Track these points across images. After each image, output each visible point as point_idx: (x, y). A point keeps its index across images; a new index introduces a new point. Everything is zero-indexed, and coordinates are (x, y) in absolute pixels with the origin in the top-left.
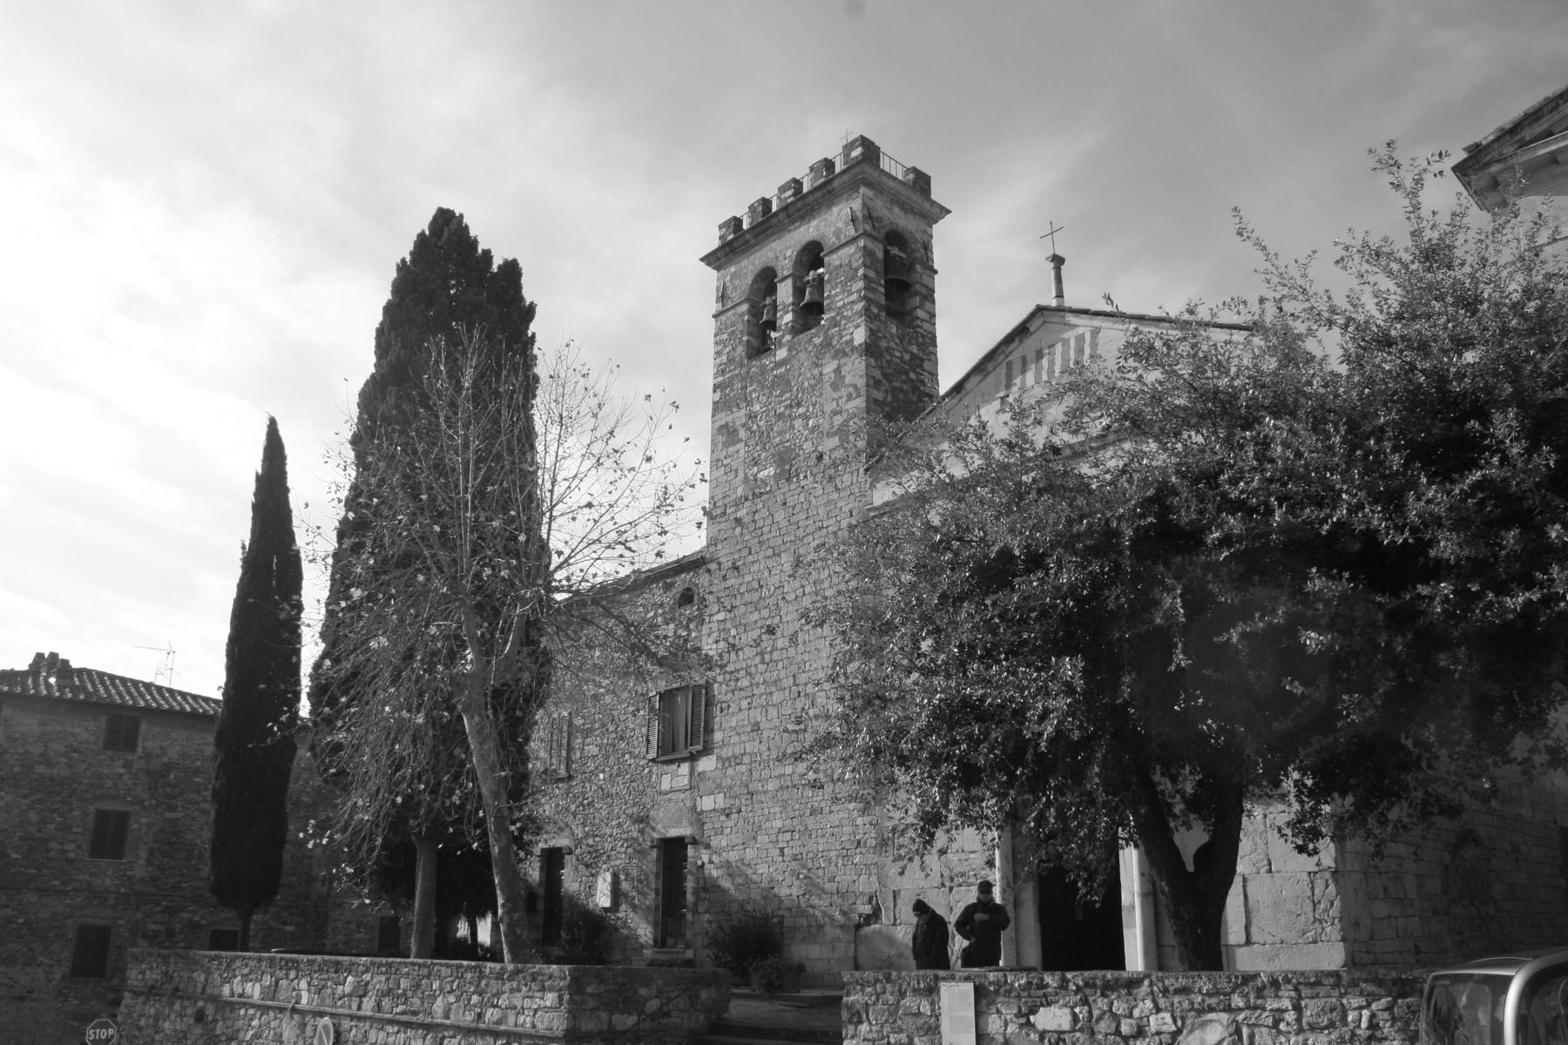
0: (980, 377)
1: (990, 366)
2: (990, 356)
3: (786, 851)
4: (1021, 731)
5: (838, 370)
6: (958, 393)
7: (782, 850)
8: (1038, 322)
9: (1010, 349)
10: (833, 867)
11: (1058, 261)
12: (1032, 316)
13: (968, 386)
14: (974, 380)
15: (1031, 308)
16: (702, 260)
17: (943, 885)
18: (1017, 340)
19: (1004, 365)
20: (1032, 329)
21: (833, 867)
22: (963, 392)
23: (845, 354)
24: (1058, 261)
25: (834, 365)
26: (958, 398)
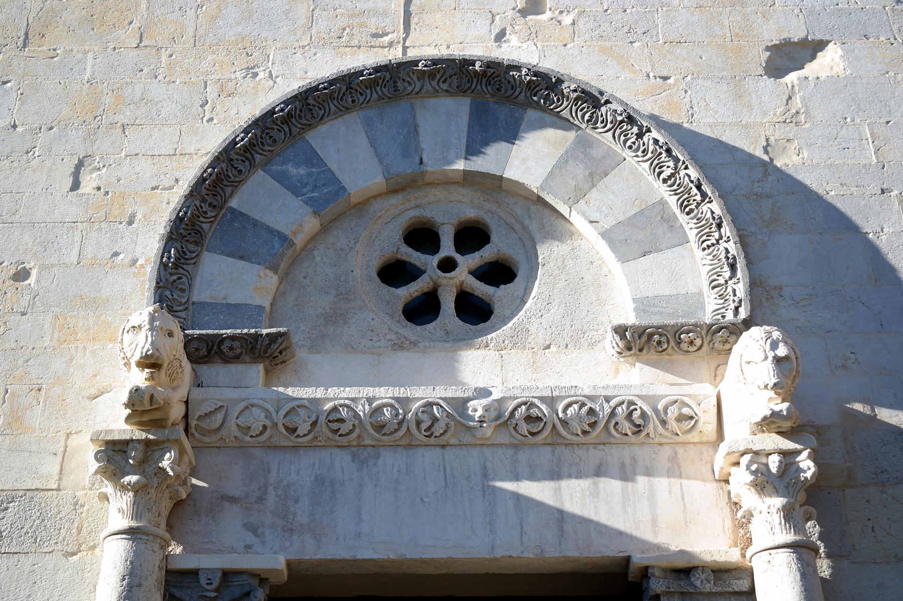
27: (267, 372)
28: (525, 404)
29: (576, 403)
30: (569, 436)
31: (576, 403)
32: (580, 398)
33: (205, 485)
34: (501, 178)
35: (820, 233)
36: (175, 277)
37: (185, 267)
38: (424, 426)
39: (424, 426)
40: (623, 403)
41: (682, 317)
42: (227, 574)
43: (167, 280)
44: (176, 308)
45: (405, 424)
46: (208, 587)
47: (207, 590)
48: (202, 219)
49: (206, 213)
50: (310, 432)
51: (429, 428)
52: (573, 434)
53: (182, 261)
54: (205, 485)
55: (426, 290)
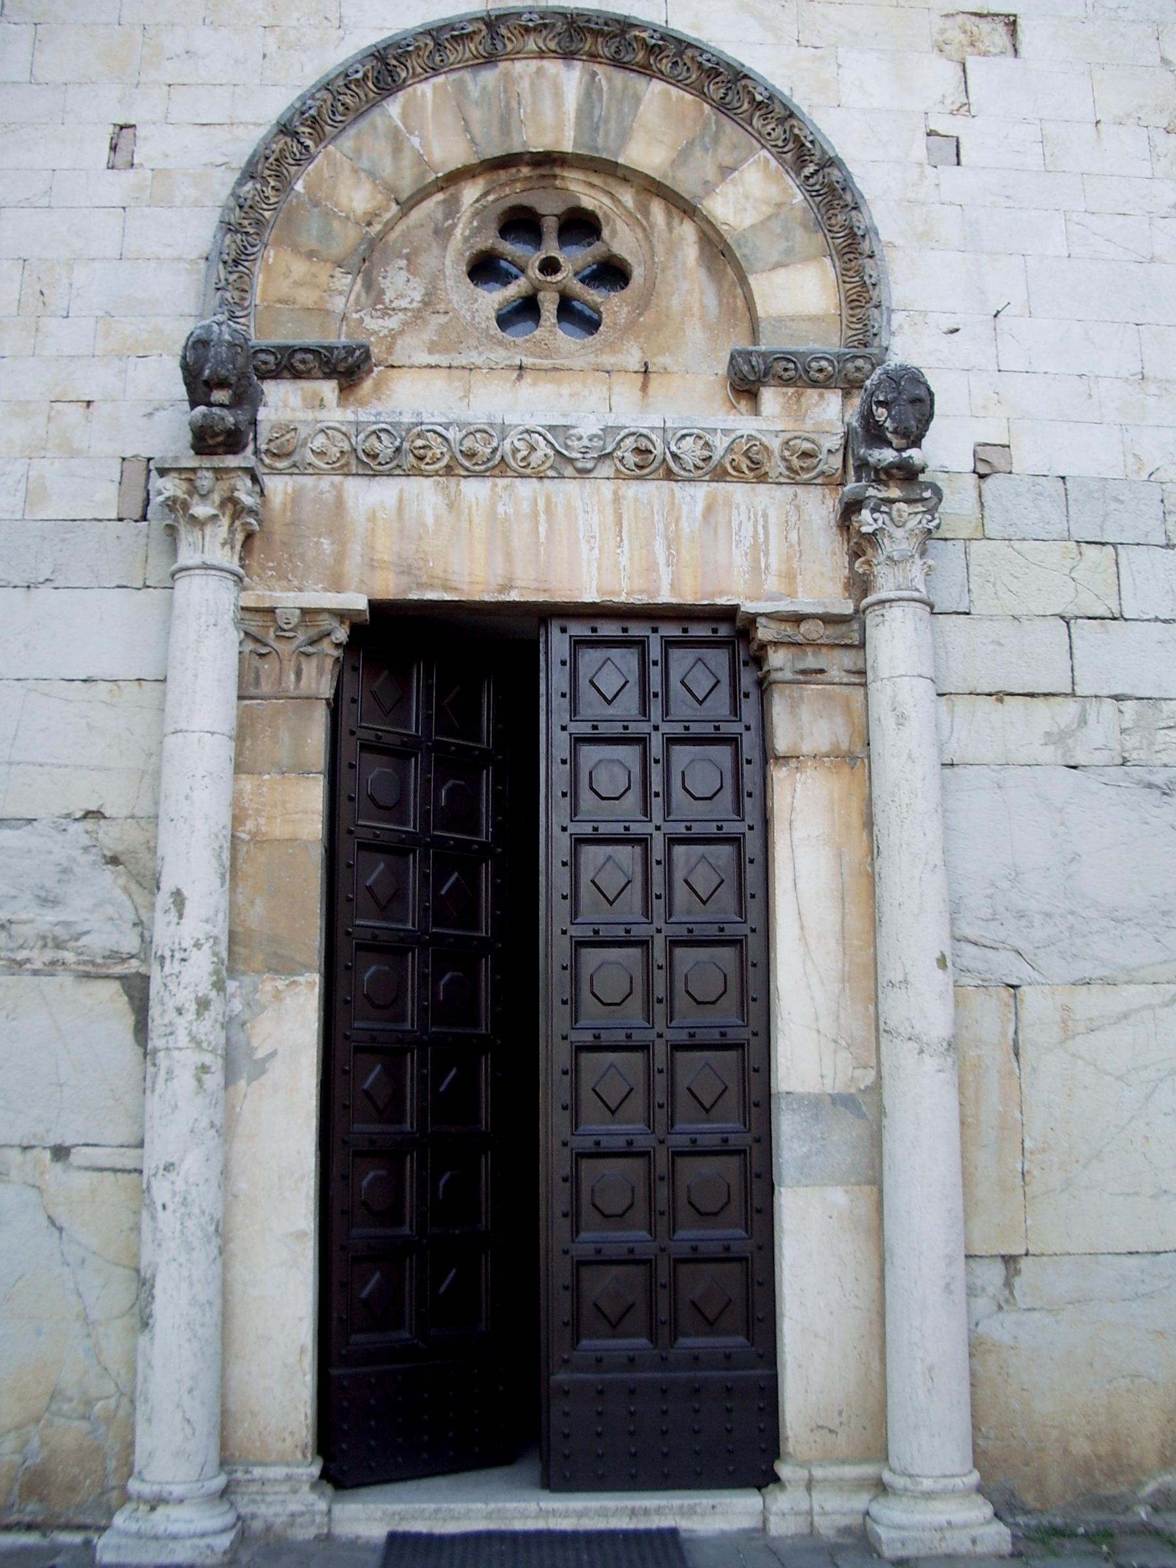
27: (341, 390)
28: (633, 434)
29: (690, 435)
30: (682, 473)
31: (690, 435)
32: (695, 431)
33: (454, 1271)
34: (616, 163)
35: (697, 1453)
36: (235, 276)
37: (246, 264)
38: (520, 456)
39: (520, 456)
40: (742, 437)
41: (814, 341)
42: (305, 612)
43: (226, 280)
44: (238, 314)
45: (499, 454)
46: (286, 627)
47: (285, 630)
48: (265, 206)
49: (267, 198)
50: (392, 460)
51: (524, 459)
52: (684, 469)
53: (243, 257)
54: (454, 1271)
55: (524, 294)
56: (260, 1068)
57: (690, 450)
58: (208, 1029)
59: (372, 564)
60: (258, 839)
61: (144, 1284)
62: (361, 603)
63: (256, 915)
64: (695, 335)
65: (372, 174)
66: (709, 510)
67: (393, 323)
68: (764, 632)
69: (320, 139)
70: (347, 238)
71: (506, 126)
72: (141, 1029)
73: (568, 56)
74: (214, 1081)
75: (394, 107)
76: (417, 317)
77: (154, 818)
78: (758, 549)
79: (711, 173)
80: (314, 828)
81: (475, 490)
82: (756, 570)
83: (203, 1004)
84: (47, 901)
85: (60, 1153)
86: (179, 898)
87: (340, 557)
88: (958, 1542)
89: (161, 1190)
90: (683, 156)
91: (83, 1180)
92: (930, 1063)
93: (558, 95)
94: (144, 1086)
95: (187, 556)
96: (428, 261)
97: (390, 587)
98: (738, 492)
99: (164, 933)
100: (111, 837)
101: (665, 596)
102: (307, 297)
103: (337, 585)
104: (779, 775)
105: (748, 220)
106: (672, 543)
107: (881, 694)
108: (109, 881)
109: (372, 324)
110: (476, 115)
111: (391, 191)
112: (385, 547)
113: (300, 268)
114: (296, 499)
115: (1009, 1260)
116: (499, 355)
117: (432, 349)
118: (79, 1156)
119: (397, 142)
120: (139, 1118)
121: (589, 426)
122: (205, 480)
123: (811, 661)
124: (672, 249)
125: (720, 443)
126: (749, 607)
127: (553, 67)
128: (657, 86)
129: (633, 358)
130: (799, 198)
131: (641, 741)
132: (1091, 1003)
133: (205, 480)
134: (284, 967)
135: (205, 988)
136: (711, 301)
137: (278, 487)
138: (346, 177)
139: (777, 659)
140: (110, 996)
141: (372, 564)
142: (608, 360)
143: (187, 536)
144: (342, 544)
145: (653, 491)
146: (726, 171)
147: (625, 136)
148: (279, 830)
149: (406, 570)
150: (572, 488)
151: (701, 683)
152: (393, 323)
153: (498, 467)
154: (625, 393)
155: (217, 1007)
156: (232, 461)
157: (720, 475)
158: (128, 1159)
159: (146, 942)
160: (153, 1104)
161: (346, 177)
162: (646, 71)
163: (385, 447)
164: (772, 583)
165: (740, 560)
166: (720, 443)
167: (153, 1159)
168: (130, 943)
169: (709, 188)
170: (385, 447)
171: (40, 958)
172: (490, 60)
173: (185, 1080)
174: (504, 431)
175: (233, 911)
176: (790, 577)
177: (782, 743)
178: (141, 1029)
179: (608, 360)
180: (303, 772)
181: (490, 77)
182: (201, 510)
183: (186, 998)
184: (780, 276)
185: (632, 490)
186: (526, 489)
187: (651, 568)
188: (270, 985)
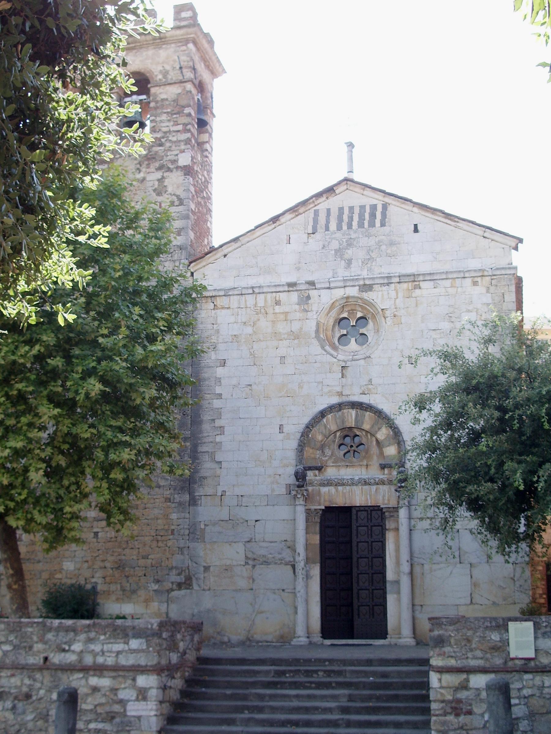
0: (293, 215)
1: (301, 210)
2: (304, 203)
3: (100, 535)
4: (39, 148)
5: (161, 180)
6: (274, 223)
7: (96, 534)
8: (342, 188)
9: (318, 201)
10: (147, 548)
11: (351, 145)
12: (339, 183)
13: (283, 219)
14: (288, 216)
15: (342, 178)
16: (346, 143)
17: (247, 563)
18: (325, 195)
19: (312, 211)
20: (337, 192)
21: (147, 548)
22: (278, 223)
23: (169, 170)
24: (351, 145)
25: (159, 175)
26: (273, 226)
56: (312, 577)
57: (372, 481)
58: (304, 572)
59: (325, 501)
60: (310, 544)
61: (296, 608)
62: (323, 508)
63: (310, 555)
64: (375, 458)
65: (322, 433)
66: (376, 490)
67: (327, 458)
68: (384, 510)
69: (313, 427)
70: (318, 445)
71: (343, 422)
72: (294, 572)
73: (353, 408)
74: (305, 580)
75: (325, 420)
76: (330, 457)
77: (295, 541)
78: (384, 496)
79: (377, 429)
80: (318, 542)
81: (340, 488)
82: (383, 499)
83: (303, 569)
84: (280, 553)
85: (283, 590)
86: (299, 554)
87: (320, 500)
88: (408, 644)
89: (298, 595)
90: (372, 426)
91: (286, 594)
92: (405, 576)
93: (351, 416)
94: (295, 580)
95: (297, 503)
96: (332, 447)
97: (328, 504)
98: (381, 487)
99: (297, 559)
100: (288, 544)
101: (369, 505)
102: (313, 456)
103: (320, 505)
104: (387, 532)
105: (383, 438)
106: (370, 496)
107: (400, 521)
108: (288, 551)
109: (323, 459)
110: (338, 421)
111: (325, 436)
112: (327, 498)
113: (311, 451)
114: (313, 490)
115: (421, 606)
116: (343, 463)
117: (333, 463)
118: (286, 591)
119: (325, 427)
120: (295, 585)
121: (357, 478)
122: (299, 491)
123: (392, 514)
124: (372, 442)
125: (377, 480)
126: (382, 506)
127: (350, 410)
128: (368, 413)
129: (365, 463)
130: (392, 433)
131: (367, 526)
132: (435, 567)
133: (299, 491)
134: (314, 563)
135: (303, 566)
136: (378, 452)
137: (310, 489)
138: (318, 434)
139: (386, 514)
140: (289, 568)
141: (325, 501)
142: (361, 463)
143: (297, 500)
144: (320, 498)
145: (366, 487)
146: (379, 429)
147: (363, 423)
148: (313, 542)
149: (330, 501)
150: (355, 487)
151: (377, 516)
152: (327, 458)
153: (343, 485)
154: (364, 470)
155: (305, 569)
156: (303, 489)
157: (378, 484)
158: (293, 591)
159: (294, 559)
160: (297, 583)
161: (318, 434)
162: (366, 410)
163: (326, 482)
164: (386, 502)
165: (381, 498)
166: (377, 480)
167: (297, 590)
168: (292, 559)
169: (376, 432)
170: (326, 482)
171: (279, 562)
172: (340, 410)
173: (301, 579)
174: (344, 479)
175: (307, 555)
176: (389, 500)
177: (387, 527)
178: (294, 572)
179: (361, 463)
180: (316, 533)
181: (340, 413)
182: (299, 496)
183: (300, 568)
184: (388, 448)
185: (365, 487)
186: (348, 488)
187: (367, 500)
188: (312, 565)
